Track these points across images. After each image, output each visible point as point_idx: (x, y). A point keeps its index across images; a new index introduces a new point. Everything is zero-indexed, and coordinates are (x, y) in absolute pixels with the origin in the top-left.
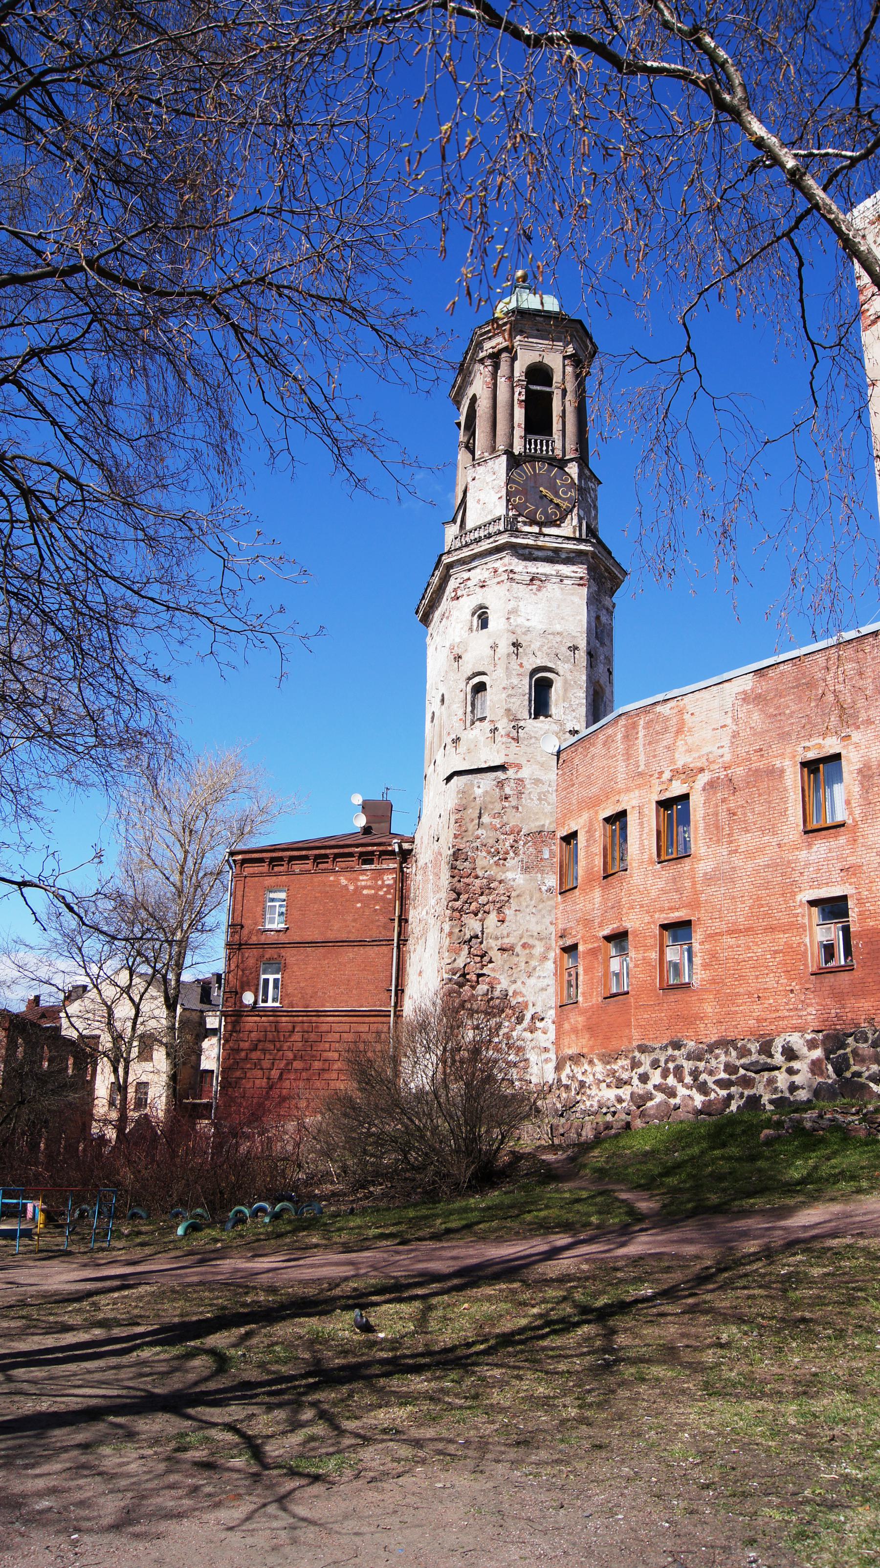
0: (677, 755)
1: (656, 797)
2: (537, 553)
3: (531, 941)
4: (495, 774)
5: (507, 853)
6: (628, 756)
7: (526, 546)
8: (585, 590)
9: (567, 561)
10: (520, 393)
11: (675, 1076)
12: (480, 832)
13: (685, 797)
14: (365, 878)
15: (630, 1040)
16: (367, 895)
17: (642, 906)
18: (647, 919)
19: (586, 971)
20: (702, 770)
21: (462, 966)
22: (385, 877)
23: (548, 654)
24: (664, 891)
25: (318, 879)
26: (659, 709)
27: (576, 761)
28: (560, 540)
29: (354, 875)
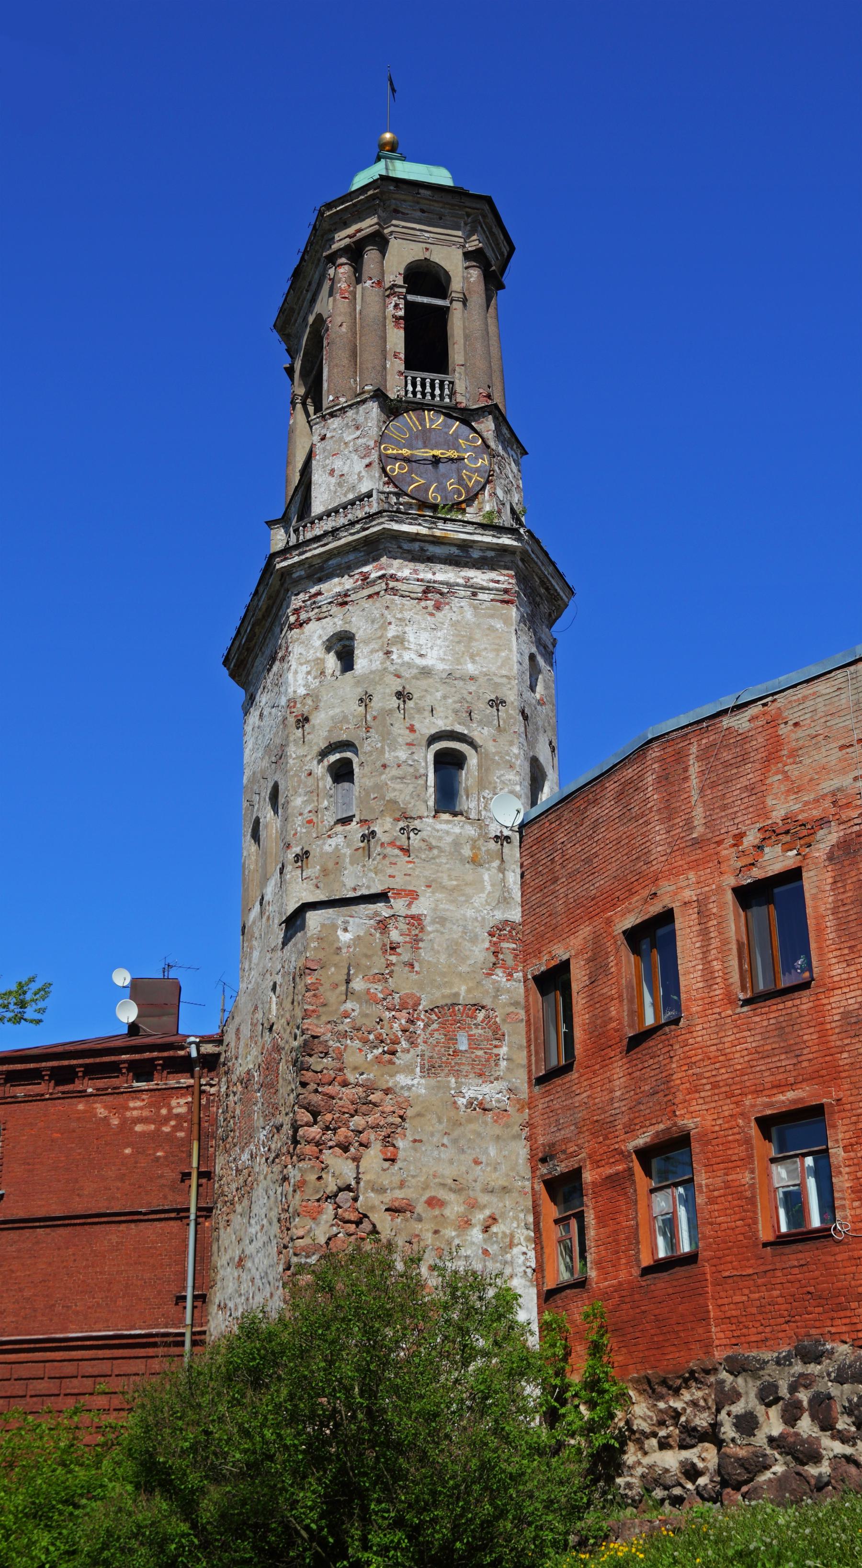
0: (770, 801)
1: (731, 881)
2: (432, 550)
3: (442, 1194)
4: (372, 908)
5: (396, 1042)
6: (669, 812)
7: (415, 538)
8: (513, 612)
9: (481, 564)
10: (396, 306)
11: (813, 1417)
12: (349, 1005)
13: (794, 875)
14: (139, 1104)
15: (708, 1346)
16: (143, 1134)
17: (715, 1086)
18: (728, 1109)
19: (601, 1221)
20: (822, 822)
21: (322, 1240)
22: (174, 1102)
23: (456, 712)
24: (759, 1053)
25: (60, 1106)
26: (726, 722)
27: (561, 837)
28: (470, 529)
29: (121, 1099)
